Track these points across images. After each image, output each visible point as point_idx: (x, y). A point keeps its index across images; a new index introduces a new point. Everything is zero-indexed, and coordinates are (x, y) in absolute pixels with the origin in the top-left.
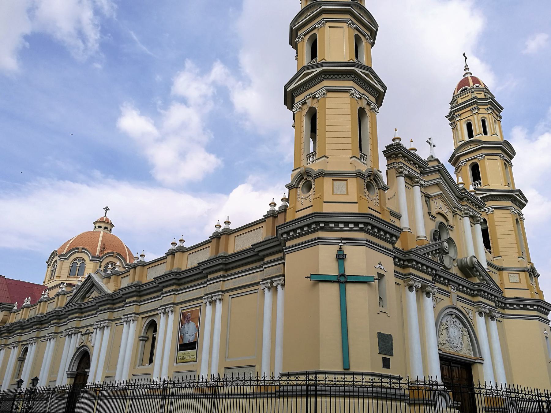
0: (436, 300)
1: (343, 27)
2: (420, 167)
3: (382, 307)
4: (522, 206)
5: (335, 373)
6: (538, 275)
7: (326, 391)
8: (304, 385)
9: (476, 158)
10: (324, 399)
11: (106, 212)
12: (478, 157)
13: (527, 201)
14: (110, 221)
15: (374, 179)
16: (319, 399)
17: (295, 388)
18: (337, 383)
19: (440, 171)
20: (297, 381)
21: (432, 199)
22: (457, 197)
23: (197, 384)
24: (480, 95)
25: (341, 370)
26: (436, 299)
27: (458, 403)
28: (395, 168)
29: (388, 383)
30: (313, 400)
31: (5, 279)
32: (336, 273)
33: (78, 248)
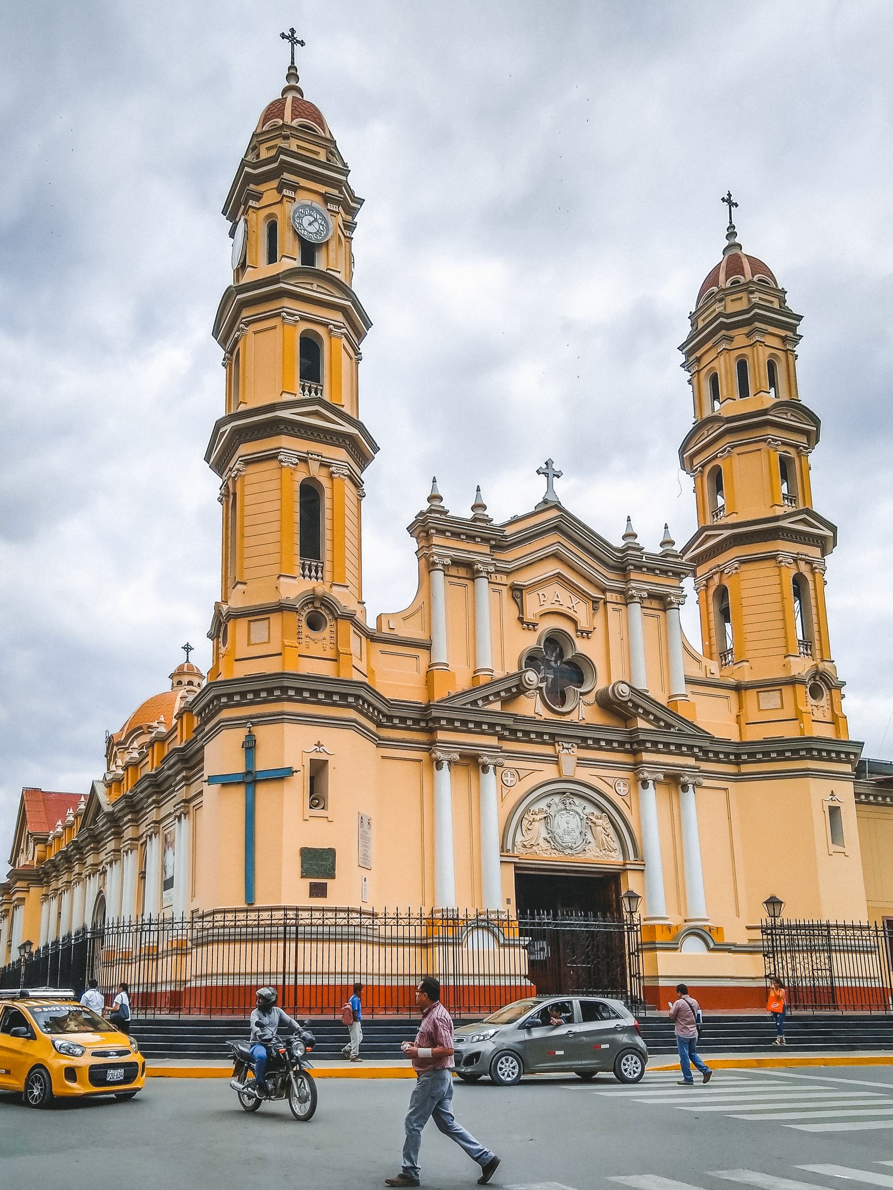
1: (275, 327)
3: (323, 808)
4: (825, 544)
5: (235, 911)
7: (271, 934)
8: (281, 925)
10: (308, 945)
11: (188, 654)
14: (195, 668)
15: (322, 604)
16: (301, 945)
17: (333, 929)
20: (271, 920)
21: (527, 591)
23: (128, 928)
24: (740, 301)
25: (244, 906)
26: (516, 771)
27: (526, 938)
28: (425, 557)
30: (293, 945)
31: (42, 792)
32: (242, 770)
33: (142, 727)
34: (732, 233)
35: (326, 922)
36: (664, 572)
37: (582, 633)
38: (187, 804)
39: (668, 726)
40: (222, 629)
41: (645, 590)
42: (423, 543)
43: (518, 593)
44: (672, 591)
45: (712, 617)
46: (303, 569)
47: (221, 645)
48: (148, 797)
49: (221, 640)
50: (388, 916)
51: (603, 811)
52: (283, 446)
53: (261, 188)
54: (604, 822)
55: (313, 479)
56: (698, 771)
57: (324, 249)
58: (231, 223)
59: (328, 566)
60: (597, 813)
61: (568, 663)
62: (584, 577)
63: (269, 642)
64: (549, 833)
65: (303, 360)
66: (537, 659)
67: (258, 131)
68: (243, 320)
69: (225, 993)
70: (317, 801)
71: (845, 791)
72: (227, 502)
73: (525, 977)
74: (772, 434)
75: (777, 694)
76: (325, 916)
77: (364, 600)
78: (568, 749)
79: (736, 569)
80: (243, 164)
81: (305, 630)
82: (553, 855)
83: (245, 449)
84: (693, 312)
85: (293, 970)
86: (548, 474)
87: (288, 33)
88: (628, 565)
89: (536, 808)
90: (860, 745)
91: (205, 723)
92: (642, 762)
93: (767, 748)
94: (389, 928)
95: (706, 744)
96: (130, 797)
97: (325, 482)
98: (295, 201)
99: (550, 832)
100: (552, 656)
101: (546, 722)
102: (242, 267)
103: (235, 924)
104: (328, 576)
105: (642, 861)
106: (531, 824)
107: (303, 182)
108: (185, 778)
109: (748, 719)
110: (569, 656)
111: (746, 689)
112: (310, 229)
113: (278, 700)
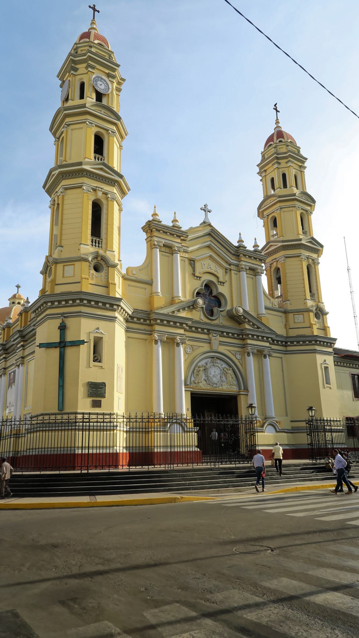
0: (193, 348)
1: (82, 128)
2: (179, 237)
5: (55, 414)
6: (327, 314)
9: (274, 212)
11: (18, 289)
12: (275, 211)
13: (322, 246)
15: (101, 259)
18: (57, 421)
19: (211, 234)
20: (110, 419)
22: (234, 254)
25: (56, 411)
29: (102, 419)
30: (87, 433)
34: (277, 122)
35: (105, 420)
36: (255, 259)
37: (221, 283)
38: (23, 359)
39: (258, 328)
40: (48, 269)
41: (248, 266)
42: (149, 235)
43: (192, 262)
44: (259, 268)
45: (273, 281)
46: (92, 242)
47: (47, 278)
48: (18, 344)
49: (47, 275)
50: (137, 417)
51: (230, 367)
52: (85, 182)
53: (77, 66)
54: (230, 372)
55: (99, 200)
56: (270, 349)
57: (107, 96)
58: (61, 82)
59: (104, 241)
60: (227, 367)
61: (215, 297)
62: (222, 259)
63: (74, 276)
64: (206, 377)
65: (96, 146)
66: (201, 294)
67: (78, 42)
68: (66, 123)
69: (94, 458)
70: (97, 358)
71: (330, 360)
72: (54, 208)
73: (196, 447)
74: (298, 204)
75: (302, 316)
76: (105, 417)
77: (121, 259)
78: (215, 337)
79: (284, 260)
80: (70, 54)
81: (93, 271)
82: (208, 387)
83: (65, 182)
84: (263, 151)
85: (87, 445)
86: (205, 210)
87: (92, 6)
88: (240, 254)
89: (200, 364)
90: (335, 340)
91: (38, 317)
92: (247, 344)
93: (299, 339)
94: (144, 423)
95: (273, 336)
96: (5, 345)
97: (104, 201)
98: (94, 74)
99: (207, 376)
100: (207, 292)
101: (205, 323)
102: (67, 99)
103: (43, 422)
104: (104, 245)
105: (247, 390)
106: (198, 372)
107: (98, 66)
108: (23, 346)
109: (290, 326)
110: (214, 293)
111: (289, 313)
112: (101, 87)
113: (79, 305)
